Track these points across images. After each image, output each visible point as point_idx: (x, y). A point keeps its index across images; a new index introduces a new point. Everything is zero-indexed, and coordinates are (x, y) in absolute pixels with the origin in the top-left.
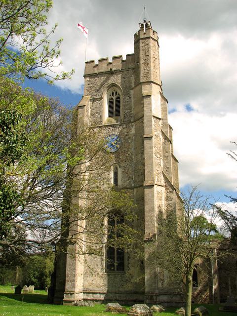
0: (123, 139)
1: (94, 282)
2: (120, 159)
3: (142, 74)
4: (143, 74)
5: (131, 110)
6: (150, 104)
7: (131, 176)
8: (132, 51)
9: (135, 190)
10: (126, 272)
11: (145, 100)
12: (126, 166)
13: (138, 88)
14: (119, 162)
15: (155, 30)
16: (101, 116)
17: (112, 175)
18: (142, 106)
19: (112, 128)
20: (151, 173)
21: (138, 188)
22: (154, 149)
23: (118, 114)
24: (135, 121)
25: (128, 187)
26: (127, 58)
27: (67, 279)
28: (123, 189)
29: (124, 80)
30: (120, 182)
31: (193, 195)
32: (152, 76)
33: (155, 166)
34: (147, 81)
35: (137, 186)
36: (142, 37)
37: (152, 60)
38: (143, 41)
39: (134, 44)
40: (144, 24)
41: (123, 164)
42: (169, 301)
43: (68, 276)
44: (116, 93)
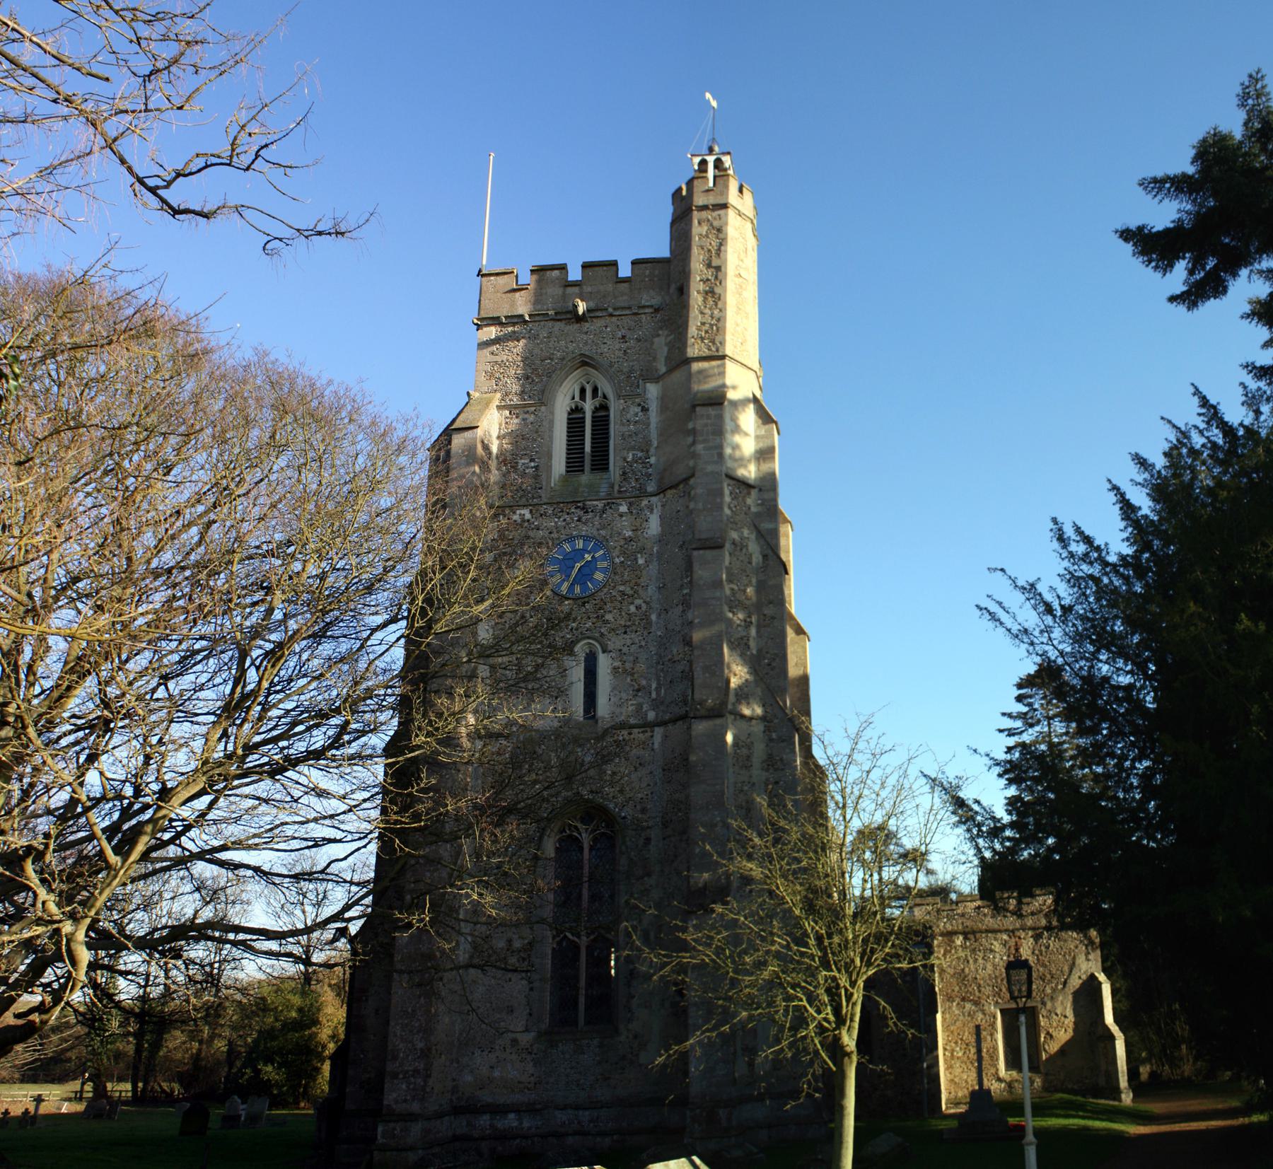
0: (616, 552)
1: (496, 1074)
2: (607, 622)
3: (692, 330)
4: (699, 329)
5: (647, 451)
7: (644, 682)
8: (661, 249)
9: (659, 732)
11: (700, 421)
12: (625, 650)
13: (678, 376)
14: (602, 635)
15: (239, 203)
17: (577, 674)
18: (690, 439)
21: (670, 726)
23: (601, 463)
24: (661, 491)
25: (632, 721)
26: (632, 270)
27: (390, 1067)
28: (613, 727)
30: (604, 706)
31: (861, 745)
35: (667, 717)
36: (700, 203)
38: (704, 214)
39: (673, 223)
40: (711, 159)
41: (615, 642)
43: (395, 1058)
44: (595, 390)
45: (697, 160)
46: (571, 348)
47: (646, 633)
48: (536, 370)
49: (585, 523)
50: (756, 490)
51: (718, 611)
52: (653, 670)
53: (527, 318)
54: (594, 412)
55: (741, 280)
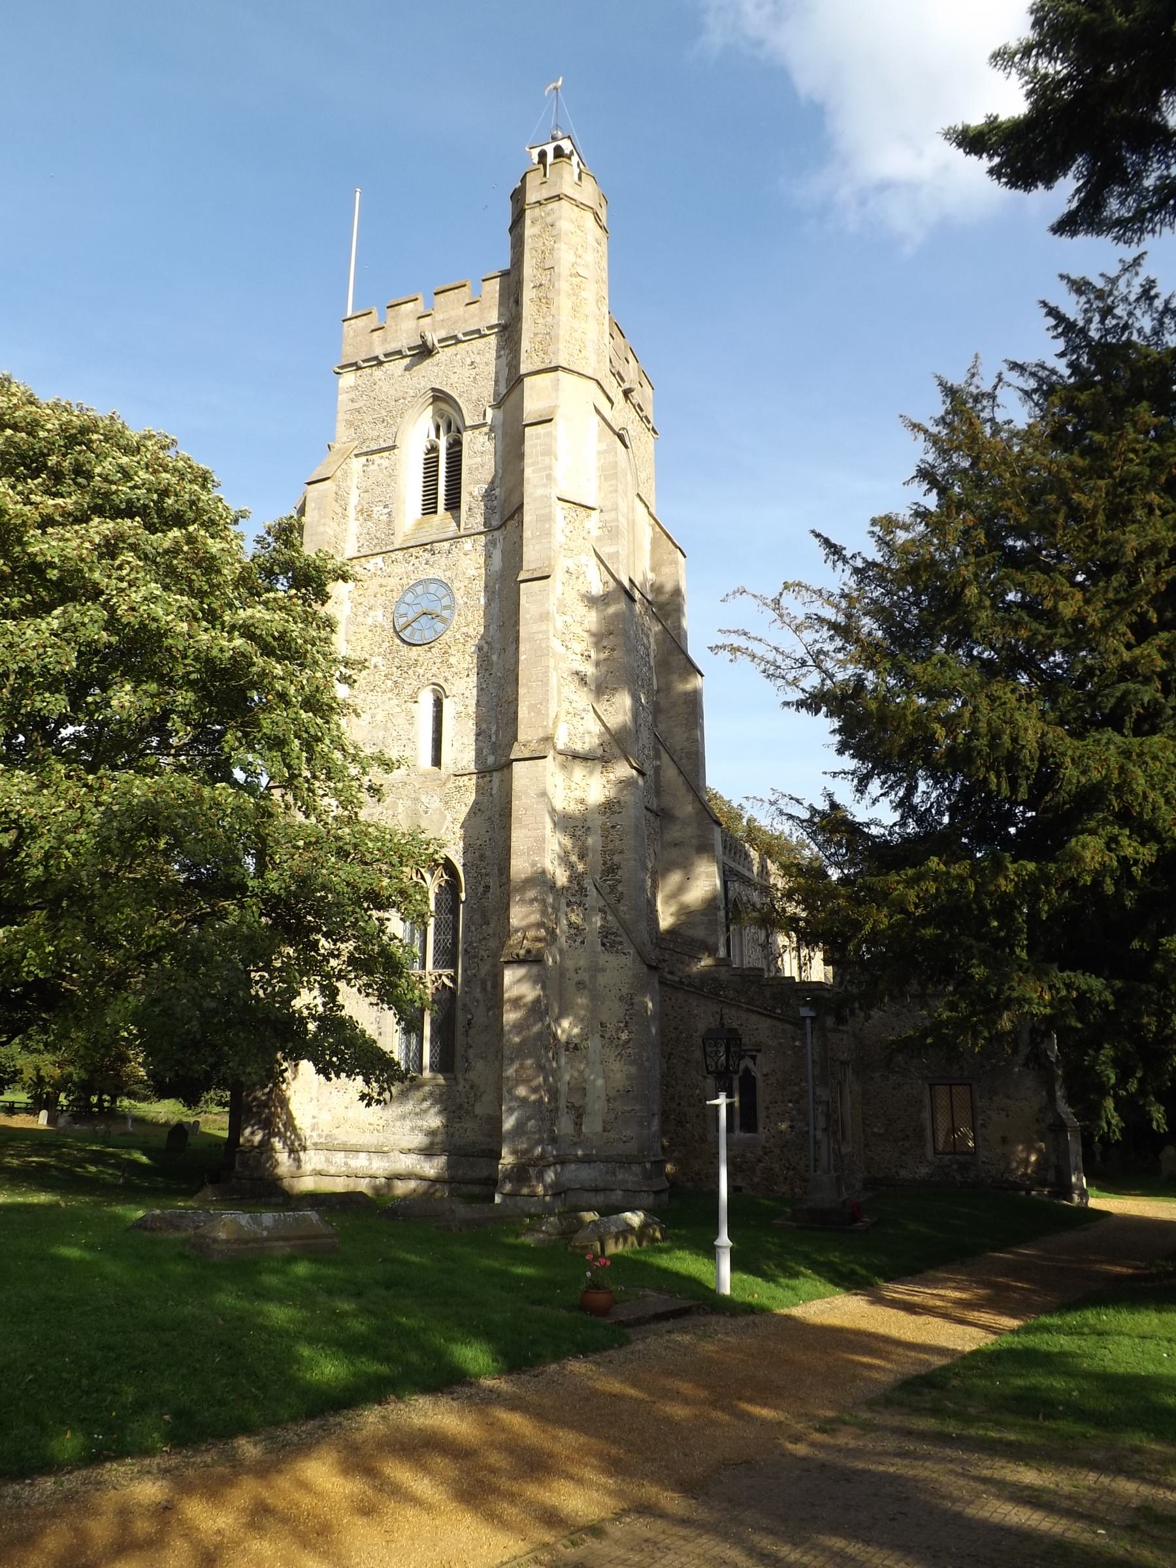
6: (549, 452)
10: (460, 1076)
16: (389, 514)
19: (427, 555)
20: (539, 712)
22: (559, 621)
23: (453, 504)
29: (473, 372)
32: (561, 346)
33: (560, 685)
34: (543, 366)
37: (564, 285)
42: (601, 1185)
45: (535, 153)
46: (423, 383)
47: (487, 675)
48: (390, 411)
49: (432, 566)
50: (597, 512)
51: (544, 645)
52: (493, 713)
53: (382, 358)
54: (448, 449)
55: (579, 279)
